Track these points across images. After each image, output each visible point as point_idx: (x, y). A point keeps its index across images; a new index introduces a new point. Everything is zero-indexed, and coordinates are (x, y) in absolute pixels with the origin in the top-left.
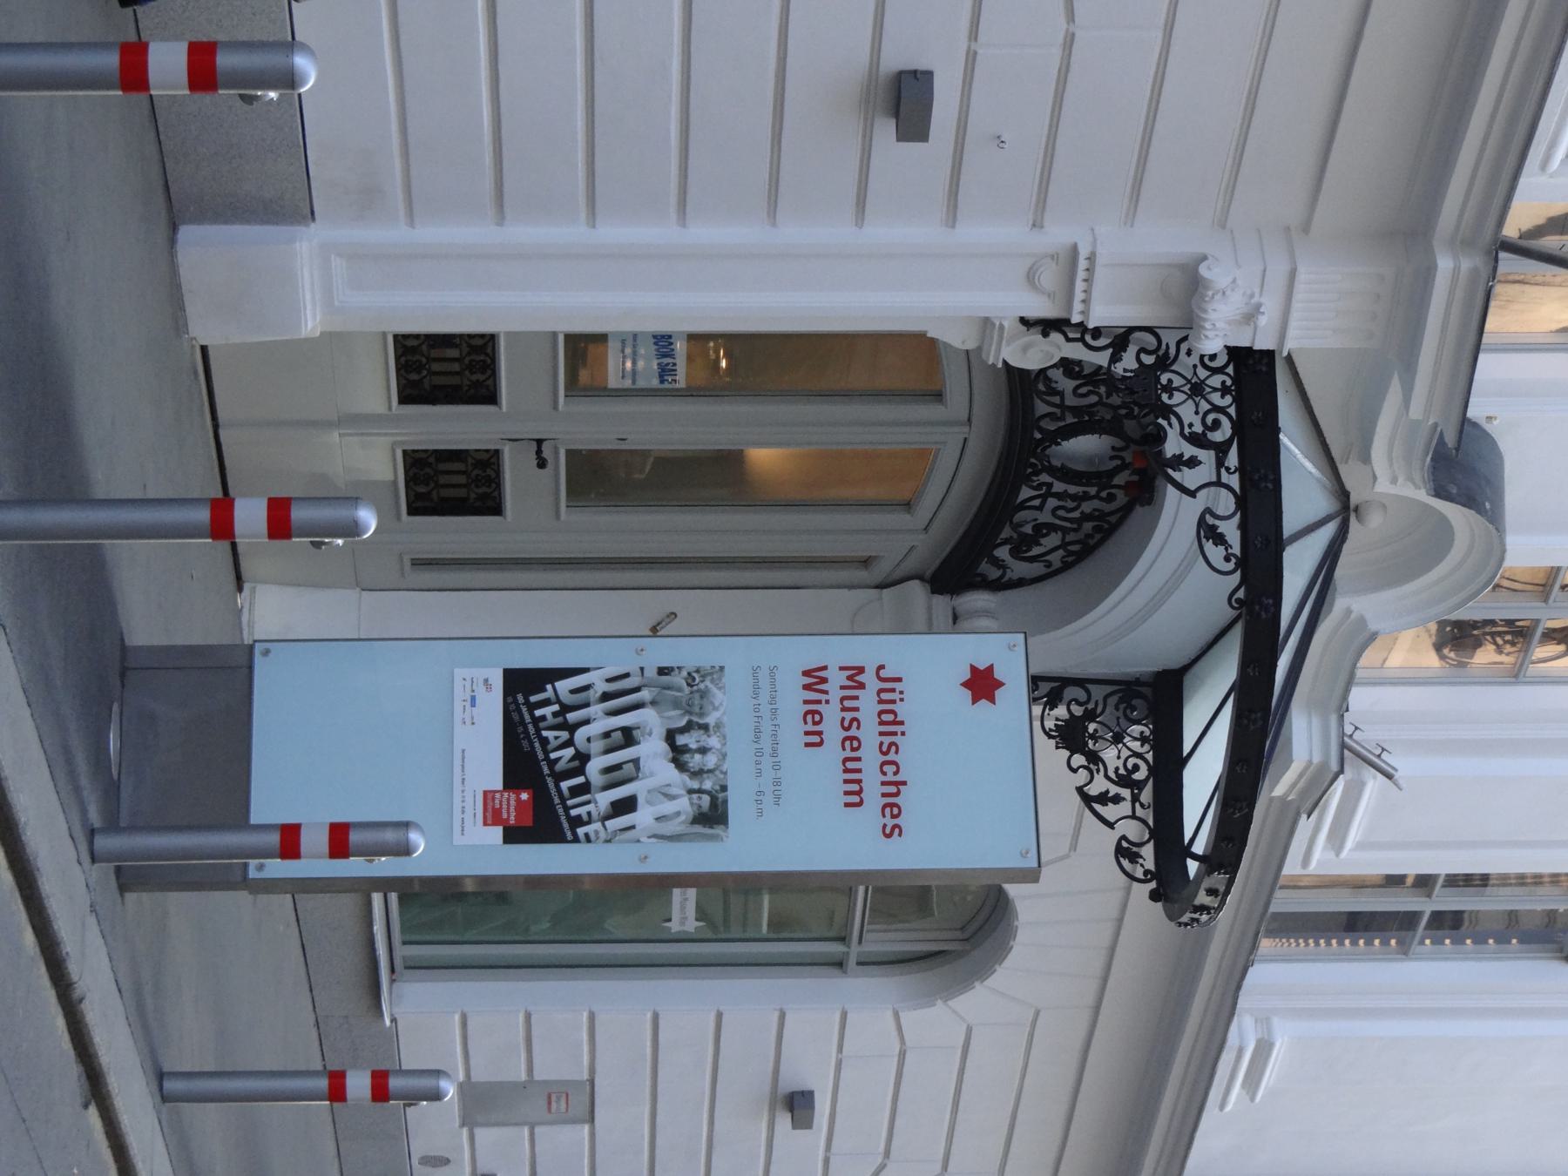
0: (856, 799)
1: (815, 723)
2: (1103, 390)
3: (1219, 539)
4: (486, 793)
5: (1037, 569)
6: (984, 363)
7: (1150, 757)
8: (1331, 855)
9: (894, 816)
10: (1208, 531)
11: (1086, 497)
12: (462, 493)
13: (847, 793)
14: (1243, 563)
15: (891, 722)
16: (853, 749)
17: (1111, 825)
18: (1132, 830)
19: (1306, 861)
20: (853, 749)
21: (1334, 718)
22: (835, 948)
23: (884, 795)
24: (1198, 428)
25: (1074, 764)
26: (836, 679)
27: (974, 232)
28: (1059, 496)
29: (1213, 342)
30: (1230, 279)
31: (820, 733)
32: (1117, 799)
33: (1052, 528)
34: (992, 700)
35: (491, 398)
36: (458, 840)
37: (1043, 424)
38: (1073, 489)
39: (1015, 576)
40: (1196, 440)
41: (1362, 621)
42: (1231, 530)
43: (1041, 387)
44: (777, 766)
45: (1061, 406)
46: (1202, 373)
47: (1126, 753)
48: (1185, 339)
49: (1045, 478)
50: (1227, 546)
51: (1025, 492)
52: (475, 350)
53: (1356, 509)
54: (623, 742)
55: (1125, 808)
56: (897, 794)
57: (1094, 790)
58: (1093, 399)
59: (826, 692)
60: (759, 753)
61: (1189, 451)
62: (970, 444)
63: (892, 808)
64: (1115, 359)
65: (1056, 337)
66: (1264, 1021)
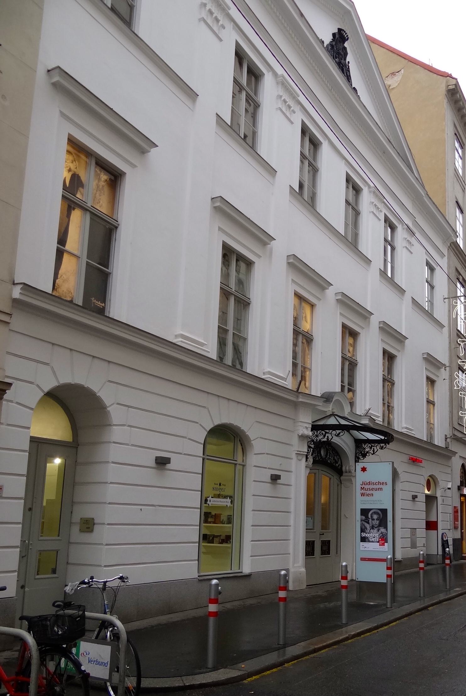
1: (369, 495)
2: (315, 450)
3: (339, 433)
4: (380, 545)
5: (339, 460)
10: (338, 435)
11: (330, 452)
12: (327, 546)
14: (343, 430)
15: (369, 483)
16: (374, 489)
17: (378, 450)
18: (378, 447)
19: (381, 421)
20: (374, 489)
21: (362, 417)
24: (323, 436)
26: (363, 491)
27: (293, 469)
28: (329, 457)
30: (301, 431)
32: (374, 449)
33: (334, 458)
35: (314, 541)
37: (319, 458)
40: (324, 436)
42: (338, 431)
44: (376, 501)
45: (317, 456)
47: (367, 448)
48: (309, 437)
49: (327, 459)
51: (329, 461)
53: (333, 413)
55: (375, 448)
57: (372, 453)
58: (316, 451)
60: (374, 503)
61: (326, 437)
63: (383, 484)
64: (312, 448)
66: (403, 428)
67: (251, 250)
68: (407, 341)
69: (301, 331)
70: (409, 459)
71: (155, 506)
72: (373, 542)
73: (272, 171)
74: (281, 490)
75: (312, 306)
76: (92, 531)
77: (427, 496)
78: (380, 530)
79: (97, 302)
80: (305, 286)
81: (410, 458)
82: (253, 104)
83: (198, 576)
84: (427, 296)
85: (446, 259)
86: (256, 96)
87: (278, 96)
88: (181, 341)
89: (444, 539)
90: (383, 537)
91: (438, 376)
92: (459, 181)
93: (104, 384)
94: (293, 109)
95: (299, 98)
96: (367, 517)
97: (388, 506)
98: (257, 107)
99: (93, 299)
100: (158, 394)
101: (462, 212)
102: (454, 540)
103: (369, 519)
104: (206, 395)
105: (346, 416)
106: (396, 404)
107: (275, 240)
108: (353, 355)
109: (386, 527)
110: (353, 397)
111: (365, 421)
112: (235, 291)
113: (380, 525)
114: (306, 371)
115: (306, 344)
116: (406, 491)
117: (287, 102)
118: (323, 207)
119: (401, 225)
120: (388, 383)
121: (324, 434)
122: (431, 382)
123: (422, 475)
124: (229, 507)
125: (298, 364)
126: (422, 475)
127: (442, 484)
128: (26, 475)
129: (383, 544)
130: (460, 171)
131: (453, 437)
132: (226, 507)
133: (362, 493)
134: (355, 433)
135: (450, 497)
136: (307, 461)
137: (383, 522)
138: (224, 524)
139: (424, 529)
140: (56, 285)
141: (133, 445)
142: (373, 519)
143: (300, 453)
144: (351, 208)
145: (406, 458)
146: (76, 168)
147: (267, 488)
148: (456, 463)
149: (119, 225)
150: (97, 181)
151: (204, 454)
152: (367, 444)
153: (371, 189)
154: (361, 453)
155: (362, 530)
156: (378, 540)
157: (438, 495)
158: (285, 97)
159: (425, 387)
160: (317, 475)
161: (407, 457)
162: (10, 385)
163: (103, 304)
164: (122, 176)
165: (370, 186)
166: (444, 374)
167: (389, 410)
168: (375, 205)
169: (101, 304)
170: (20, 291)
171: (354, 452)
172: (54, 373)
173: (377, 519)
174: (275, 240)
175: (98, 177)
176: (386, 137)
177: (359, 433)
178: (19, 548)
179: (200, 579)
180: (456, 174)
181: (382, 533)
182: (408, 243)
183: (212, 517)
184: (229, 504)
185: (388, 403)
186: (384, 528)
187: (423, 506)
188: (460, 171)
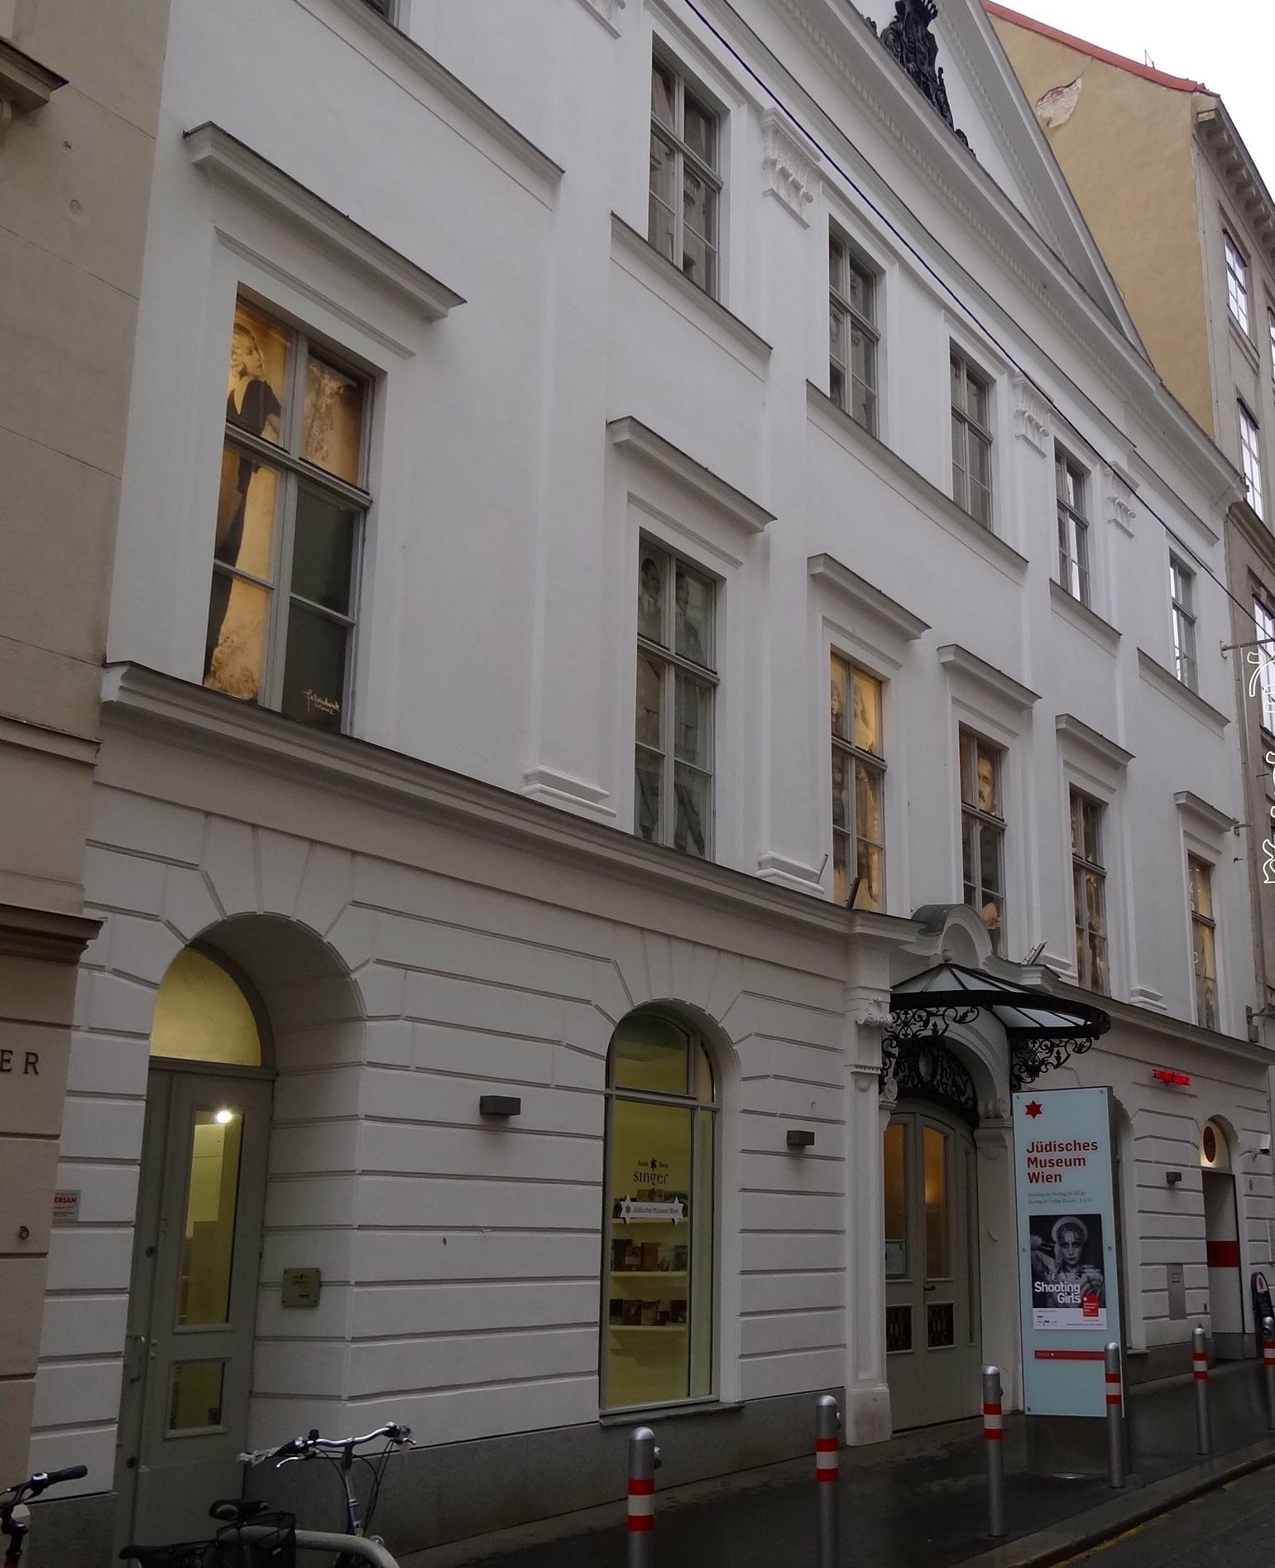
0: (1082, 1161)
3: (965, 1015)
5: (969, 1085)
7: (1041, 1040)
9: (1088, 1146)
10: (961, 1020)
11: (942, 1066)
14: (974, 1006)
15: (1050, 1147)
16: (1062, 1162)
17: (1069, 1055)
18: (1070, 1048)
24: (921, 1024)
26: (1033, 1169)
27: (846, 1114)
28: (942, 1077)
29: (889, 1018)
31: (1056, 1176)
32: (1058, 1053)
33: (954, 1080)
34: (1027, 1106)
36: (1104, 1328)
38: (939, 1072)
39: (971, 1094)
41: (988, 958)
42: (961, 1010)
46: (899, 1021)
47: (1040, 1050)
48: (886, 1029)
49: (935, 1083)
50: (968, 1011)
51: (941, 1090)
53: (946, 961)
54: (1237, 1268)
57: (1055, 1063)
58: (906, 1064)
59: (1039, 1173)
63: (1085, 1146)
64: (894, 1056)
65: (885, 1080)
66: (1133, 993)
72: (1065, 1306)
74: (817, 1174)
75: (880, 683)
76: (314, 1304)
77: (1207, 1174)
81: (1155, 1074)
83: (600, 1417)
84: (1177, 644)
85: (1220, 545)
88: (542, 791)
89: (1260, 1290)
90: (1094, 1292)
92: (1242, 347)
94: (805, 191)
95: (819, 164)
96: (1047, 1238)
101: (1254, 425)
103: (1054, 1243)
105: (982, 967)
108: (994, 807)
109: (1099, 1265)
111: (1032, 980)
113: (1083, 1260)
118: (895, 430)
121: (924, 1019)
122: (1202, 868)
124: (679, 1223)
126: (1192, 1119)
127: (1244, 1140)
129: (1094, 1313)
131: (1266, 1012)
133: (1031, 1175)
134: (1009, 1012)
137: (1091, 1252)
138: (667, 1270)
142: (1064, 1245)
144: (967, 428)
145: (1144, 1074)
147: (778, 1170)
149: (371, 502)
150: (313, 397)
151: (607, 1086)
155: (1038, 1275)
156: (1080, 1301)
157: (1238, 1167)
158: (785, 162)
162: (96, 925)
163: (334, 704)
166: (1235, 845)
167: (1093, 947)
168: (1030, 419)
170: (121, 683)
172: (211, 887)
173: (1073, 1244)
177: (1019, 1011)
178: (122, 1359)
181: (1089, 1281)
183: (634, 1253)
184: (678, 1217)
185: (1091, 926)
186: (1094, 1268)
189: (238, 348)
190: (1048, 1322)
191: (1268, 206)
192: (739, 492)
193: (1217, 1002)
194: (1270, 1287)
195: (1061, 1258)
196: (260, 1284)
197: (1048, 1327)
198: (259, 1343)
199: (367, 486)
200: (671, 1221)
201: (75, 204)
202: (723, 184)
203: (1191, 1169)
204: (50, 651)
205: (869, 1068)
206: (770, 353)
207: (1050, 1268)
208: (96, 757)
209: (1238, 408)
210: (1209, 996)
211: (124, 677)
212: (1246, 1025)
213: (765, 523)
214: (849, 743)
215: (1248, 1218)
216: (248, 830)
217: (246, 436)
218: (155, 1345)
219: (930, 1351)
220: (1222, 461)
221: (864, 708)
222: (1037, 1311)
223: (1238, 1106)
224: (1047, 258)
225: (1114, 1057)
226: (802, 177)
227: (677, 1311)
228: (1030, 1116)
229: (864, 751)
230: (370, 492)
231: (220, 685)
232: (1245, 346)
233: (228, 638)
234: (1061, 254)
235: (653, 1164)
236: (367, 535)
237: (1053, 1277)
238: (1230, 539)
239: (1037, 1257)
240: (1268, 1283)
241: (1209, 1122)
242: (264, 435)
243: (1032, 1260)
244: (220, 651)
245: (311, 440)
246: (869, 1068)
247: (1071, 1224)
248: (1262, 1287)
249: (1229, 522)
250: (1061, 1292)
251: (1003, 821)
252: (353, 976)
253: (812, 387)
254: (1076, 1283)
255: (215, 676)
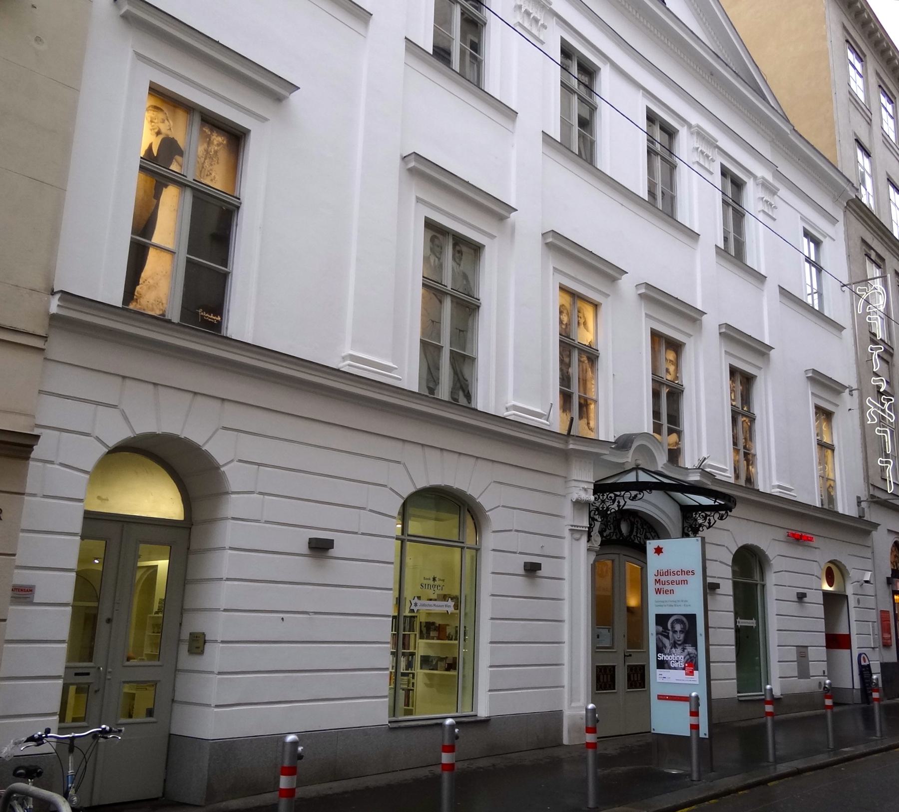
0: (686, 581)
2: (609, 523)
4: (686, 675)
6: (599, 550)
8: (729, 471)
9: (689, 572)
10: (634, 498)
13: (684, 584)
15: (668, 573)
17: (715, 521)
18: (717, 516)
22: (759, 587)
23: (685, 574)
24: (611, 501)
25: (702, 530)
26: (658, 586)
27: (566, 553)
28: (637, 533)
29: (592, 498)
31: (671, 590)
32: (709, 520)
35: (614, 667)
37: (618, 537)
40: (614, 501)
41: (664, 464)
42: (634, 493)
43: (609, 537)
44: (679, 601)
45: (613, 533)
46: (600, 500)
48: (592, 504)
49: (632, 537)
51: (636, 541)
52: (631, 670)
53: (637, 466)
56: (684, 571)
58: (611, 525)
60: (675, 605)
61: (616, 503)
62: (624, 554)
63: (688, 573)
65: (592, 534)
66: (774, 487)
67: (743, 359)
68: (294, 97)
69: (576, 344)
70: (788, 536)
71: (309, 614)
72: (675, 668)
73: (511, 114)
74: (545, 587)
75: (596, 306)
76: (202, 652)
77: (826, 594)
78: (686, 649)
79: (207, 315)
80: (580, 278)
81: (788, 535)
82: (588, 108)
83: (389, 722)
84: (809, 282)
85: (841, 226)
86: (591, 98)
87: (515, 7)
88: (349, 365)
89: (863, 663)
90: (692, 661)
91: (837, 405)
92: (859, 108)
93: (214, 433)
94: (542, 23)
95: (717, 143)
96: (665, 628)
97: (697, 609)
98: (483, 26)
99: (200, 311)
100: (315, 446)
101: (868, 154)
102: (884, 666)
103: (669, 630)
104: (490, 464)
105: (660, 469)
106: (758, 448)
107: (517, 210)
108: (677, 378)
109: (695, 645)
110: (680, 441)
111: (694, 478)
112: (451, 289)
113: (685, 641)
114: (588, 403)
115: (587, 364)
116: (785, 586)
117: (531, 13)
118: (605, 160)
119: (752, 179)
120: (744, 419)
121: (613, 498)
122: (824, 414)
123: (816, 561)
124: (451, 613)
125: (573, 393)
126: (816, 561)
127: (853, 574)
128: (75, 570)
129: (691, 673)
130: (892, 136)
131: (870, 500)
132: (445, 613)
133: (657, 589)
134: (679, 496)
135: (873, 596)
136: (590, 542)
137: (690, 637)
138: (451, 640)
139: (824, 646)
140: (136, 293)
141: (267, 522)
142: (675, 632)
143: (576, 528)
144: (577, 97)
145: (781, 534)
146: (170, 129)
147: (519, 584)
148: (882, 542)
149: (241, 203)
150: (205, 145)
151: (403, 533)
152: (608, 493)
153: (692, 130)
154: (691, 526)
155: (660, 650)
156: (683, 666)
157: (850, 591)
158: (703, 147)
159: (813, 422)
160: (617, 563)
161: (784, 532)
162: (37, 437)
163: (217, 317)
164: (247, 135)
165: (691, 125)
166: (849, 401)
167: (747, 460)
168: (702, 152)
169: (214, 318)
170: (58, 303)
171: (680, 525)
172: (126, 419)
173: (680, 631)
174: (517, 210)
175: (208, 139)
176: (711, 49)
177: (686, 496)
178: (62, 679)
179: (391, 727)
180: (884, 140)
181: (689, 654)
182: (767, 205)
183: (435, 630)
184: (451, 610)
185: (745, 447)
186: (692, 646)
187: (820, 611)
188: (892, 136)
189: (155, 119)
190: (665, 678)
191: (870, 14)
192: (490, 195)
193: (836, 493)
194: (870, 662)
195: (673, 640)
196: (179, 641)
197: (665, 681)
198: (180, 673)
199: (240, 196)
200: (446, 612)
201: (38, 39)
202: (487, 21)
203: (814, 591)
204: (17, 286)
205: (580, 527)
206: (516, 116)
207: (666, 645)
208: (44, 345)
209: (856, 145)
210: (831, 490)
211: (60, 299)
212: (857, 507)
213: (770, 351)
214: (446, 286)
215: (856, 621)
216: (151, 387)
217: (174, 175)
218: (110, 672)
219: (596, 693)
220: (838, 174)
221: (585, 321)
222: (659, 671)
223: (849, 555)
224: (731, 75)
225: (513, 469)
226: (540, 15)
227: (452, 666)
228: (654, 551)
229: (585, 345)
230: (240, 198)
231: (140, 306)
232: (862, 108)
233: (146, 280)
234: (727, 60)
235: (434, 579)
236: (238, 222)
237: (668, 651)
238: (848, 221)
239: (659, 638)
240: (870, 660)
241: (828, 564)
242: (172, 167)
243: (657, 640)
244: (140, 288)
245: (204, 169)
246: (580, 527)
247: (679, 619)
248: (865, 662)
249: (847, 212)
250: (672, 660)
251: (682, 386)
252: (222, 469)
253: (545, 135)
254: (681, 655)
255: (137, 302)
